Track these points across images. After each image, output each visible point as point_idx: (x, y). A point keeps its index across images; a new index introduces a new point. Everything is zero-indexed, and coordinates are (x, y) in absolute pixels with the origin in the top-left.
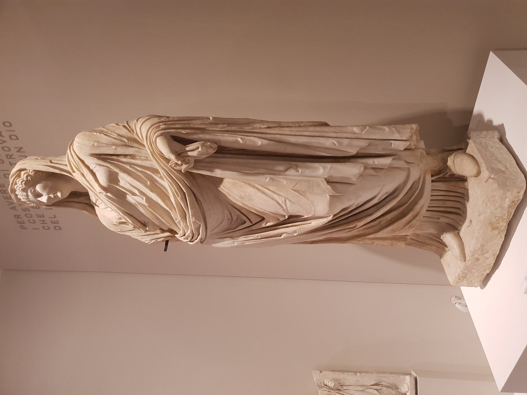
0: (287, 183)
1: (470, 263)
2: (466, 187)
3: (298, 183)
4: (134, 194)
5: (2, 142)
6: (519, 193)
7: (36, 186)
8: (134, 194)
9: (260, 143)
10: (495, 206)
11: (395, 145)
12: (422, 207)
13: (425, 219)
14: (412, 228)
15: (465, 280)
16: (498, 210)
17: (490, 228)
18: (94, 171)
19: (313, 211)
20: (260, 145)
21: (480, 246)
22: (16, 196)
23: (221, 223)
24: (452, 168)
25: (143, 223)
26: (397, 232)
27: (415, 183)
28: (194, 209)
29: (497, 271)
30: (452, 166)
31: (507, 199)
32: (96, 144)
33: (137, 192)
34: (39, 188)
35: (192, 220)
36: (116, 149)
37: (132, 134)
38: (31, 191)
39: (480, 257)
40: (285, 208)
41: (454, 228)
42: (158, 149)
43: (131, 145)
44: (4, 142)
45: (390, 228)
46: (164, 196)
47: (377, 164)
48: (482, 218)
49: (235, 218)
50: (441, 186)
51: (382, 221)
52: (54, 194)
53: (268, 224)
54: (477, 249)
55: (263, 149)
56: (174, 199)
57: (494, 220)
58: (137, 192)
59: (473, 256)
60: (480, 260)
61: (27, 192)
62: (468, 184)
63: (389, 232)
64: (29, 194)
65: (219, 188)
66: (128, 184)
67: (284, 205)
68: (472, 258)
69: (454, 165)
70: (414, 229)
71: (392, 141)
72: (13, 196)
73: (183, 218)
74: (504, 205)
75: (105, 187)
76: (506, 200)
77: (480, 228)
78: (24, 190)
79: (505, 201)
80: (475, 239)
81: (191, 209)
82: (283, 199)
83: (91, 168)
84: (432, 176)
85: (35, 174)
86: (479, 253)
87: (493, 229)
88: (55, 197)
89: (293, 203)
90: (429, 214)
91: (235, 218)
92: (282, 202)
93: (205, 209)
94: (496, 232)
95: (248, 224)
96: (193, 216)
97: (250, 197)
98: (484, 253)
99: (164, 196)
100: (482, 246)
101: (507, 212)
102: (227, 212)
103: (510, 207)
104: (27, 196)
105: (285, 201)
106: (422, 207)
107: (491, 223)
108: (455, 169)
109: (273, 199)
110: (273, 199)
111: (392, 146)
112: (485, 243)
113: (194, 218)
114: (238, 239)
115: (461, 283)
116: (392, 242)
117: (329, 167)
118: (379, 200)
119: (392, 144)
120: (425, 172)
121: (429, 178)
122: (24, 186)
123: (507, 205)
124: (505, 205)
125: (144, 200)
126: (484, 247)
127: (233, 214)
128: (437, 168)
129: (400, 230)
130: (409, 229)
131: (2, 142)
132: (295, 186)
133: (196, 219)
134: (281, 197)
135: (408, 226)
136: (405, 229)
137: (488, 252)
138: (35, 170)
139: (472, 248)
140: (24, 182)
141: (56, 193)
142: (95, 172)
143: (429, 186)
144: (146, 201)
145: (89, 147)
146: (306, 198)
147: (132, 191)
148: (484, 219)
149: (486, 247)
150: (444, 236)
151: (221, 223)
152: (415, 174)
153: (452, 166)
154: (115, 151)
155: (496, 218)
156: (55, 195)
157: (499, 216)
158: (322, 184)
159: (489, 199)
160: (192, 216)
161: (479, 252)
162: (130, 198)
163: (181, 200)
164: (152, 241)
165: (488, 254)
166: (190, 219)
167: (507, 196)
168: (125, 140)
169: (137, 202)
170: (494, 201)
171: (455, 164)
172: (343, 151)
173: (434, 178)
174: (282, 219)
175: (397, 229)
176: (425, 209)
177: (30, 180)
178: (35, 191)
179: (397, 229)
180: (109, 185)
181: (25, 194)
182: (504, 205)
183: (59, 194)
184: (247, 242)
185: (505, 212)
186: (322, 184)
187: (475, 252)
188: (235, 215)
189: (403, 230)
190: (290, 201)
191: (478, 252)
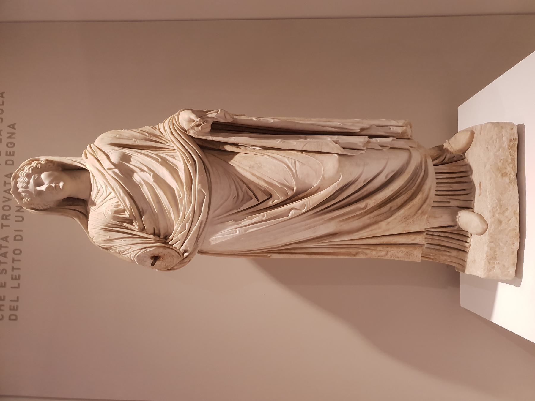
0: (297, 144)
1: (493, 227)
2: (467, 163)
3: (308, 143)
4: (142, 170)
5: (7, 199)
6: (512, 129)
7: (42, 173)
8: (142, 170)
9: (272, 121)
10: (496, 147)
11: (393, 129)
12: (430, 190)
13: (436, 204)
14: (425, 215)
15: (497, 263)
16: (500, 151)
17: (500, 175)
18: (108, 154)
19: (323, 171)
20: (272, 122)
21: (497, 201)
22: (16, 183)
23: (226, 200)
24: (448, 148)
25: (141, 210)
26: (409, 219)
27: (419, 168)
28: (202, 175)
29: (524, 257)
30: (449, 146)
31: (504, 137)
32: (118, 136)
33: (146, 169)
34: (43, 176)
35: (198, 187)
36: (135, 141)
37: (154, 129)
38: (34, 177)
39: (502, 218)
40: (294, 171)
41: (468, 207)
42: (179, 124)
43: (151, 138)
44: (9, 200)
45: (402, 212)
46: (173, 170)
47: (379, 142)
48: (488, 166)
49: (241, 195)
50: (443, 168)
51: (393, 207)
52: (56, 184)
53: (276, 201)
54: (495, 206)
55: (275, 125)
56: (184, 165)
57: (500, 164)
58: (146, 169)
59: (493, 216)
60: (503, 222)
61: (29, 179)
62: (467, 159)
63: (402, 220)
64: (32, 181)
65: (229, 162)
66: (139, 162)
67: (293, 168)
68: (493, 220)
69: (450, 144)
70: (427, 216)
71: (390, 127)
72: (13, 183)
73: (188, 188)
74: (504, 145)
75: (115, 164)
76: (504, 139)
77: (491, 179)
78: (28, 176)
79: (503, 140)
80: (489, 194)
81: (199, 175)
82: (293, 161)
83: (106, 153)
84: (433, 161)
85: (46, 163)
86: (498, 212)
87: (503, 175)
88: (56, 186)
89: (302, 163)
90: (438, 198)
91: (241, 195)
92: (292, 165)
93: (212, 180)
94: (507, 180)
95: (254, 202)
96: (199, 182)
97: (260, 165)
98: (504, 211)
99: (173, 170)
100: (499, 200)
101: (509, 154)
102: (233, 187)
103: (510, 147)
104: (28, 183)
105: (295, 162)
106: (430, 190)
107: (499, 169)
108: (452, 147)
109: (283, 162)
110: (283, 162)
111: (391, 129)
112: (500, 196)
113: (200, 185)
114: (241, 223)
115: (493, 271)
116: (407, 250)
117: (336, 138)
118: (386, 177)
119: (390, 128)
120: (426, 157)
121: (430, 163)
122: (30, 171)
123: (506, 145)
124: (505, 144)
125: (151, 176)
126: (501, 202)
127: (240, 191)
128: (435, 154)
129: (412, 217)
130: (422, 216)
131: (7, 199)
132: (305, 145)
133: (202, 187)
134: (290, 160)
135: (420, 211)
136: (418, 217)
137: (507, 209)
138: (47, 159)
139: (489, 206)
140: (32, 167)
141: (59, 183)
142: (110, 155)
143: (432, 170)
144: (153, 177)
145: (111, 138)
146: (315, 158)
147: (141, 168)
148: (491, 166)
149: (504, 201)
150: (459, 215)
151: (226, 200)
152: (416, 158)
153: (449, 146)
154: (134, 143)
155: (501, 162)
156: (58, 184)
157: (503, 159)
158: (330, 144)
159: (488, 142)
160: (198, 182)
161: (498, 209)
162: (137, 178)
163: (190, 166)
164: (140, 251)
165: (508, 211)
166: (197, 186)
167: (503, 135)
168: (147, 134)
169: (144, 181)
170: (493, 142)
171: (451, 144)
172: (347, 155)
173: (436, 162)
174: (290, 193)
175: (409, 216)
176: (433, 192)
177: (40, 167)
178: (39, 178)
179: (409, 216)
180: (119, 162)
181: (27, 180)
182: (504, 145)
183: (61, 184)
184: (251, 228)
185: (507, 153)
186: (330, 144)
187: (494, 210)
188: (242, 191)
189: (415, 217)
190: (299, 162)
191: (497, 210)
